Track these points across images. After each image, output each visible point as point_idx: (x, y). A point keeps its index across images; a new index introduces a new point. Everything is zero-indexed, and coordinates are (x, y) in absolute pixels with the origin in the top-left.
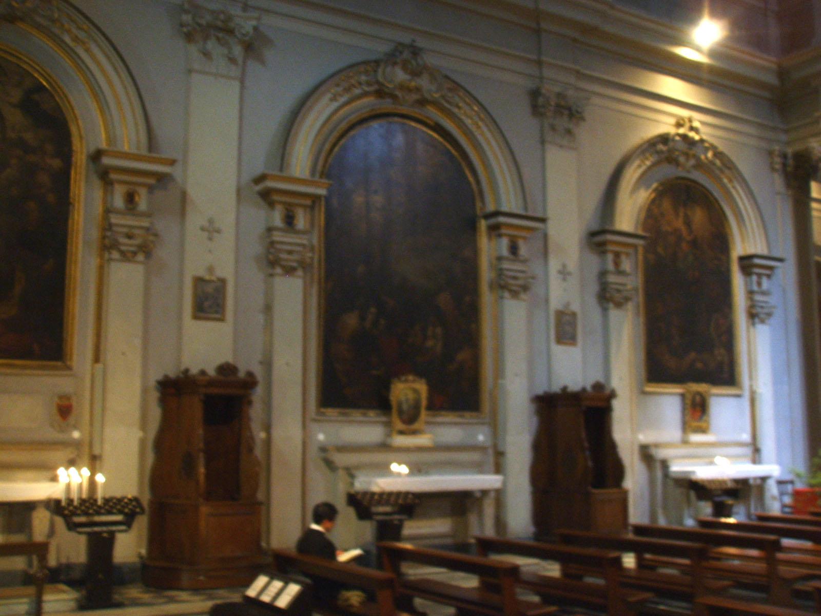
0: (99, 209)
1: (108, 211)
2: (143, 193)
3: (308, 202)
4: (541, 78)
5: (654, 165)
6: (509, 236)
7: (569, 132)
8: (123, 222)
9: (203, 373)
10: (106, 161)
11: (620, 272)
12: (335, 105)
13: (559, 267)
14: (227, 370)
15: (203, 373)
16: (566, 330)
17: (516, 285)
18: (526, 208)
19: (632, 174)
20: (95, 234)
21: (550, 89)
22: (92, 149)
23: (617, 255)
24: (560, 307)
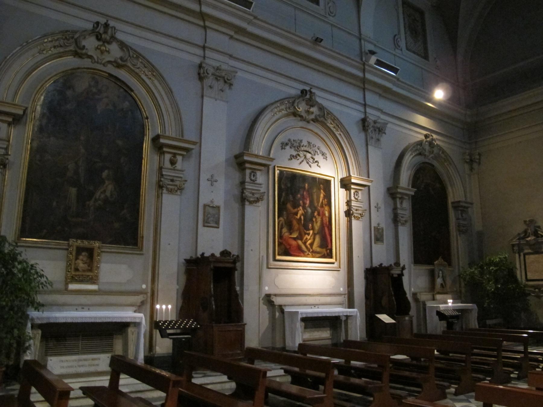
0: (156, 166)
1: (161, 168)
2: (179, 158)
3: (10, 120)
4: (204, 57)
5: (415, 156)
6: (250, 168)
7: (378, 140)
8: (401, 213)
9: (213, 255)
10: (162, 141)
11: (403, 209)
12: (40, 57)
13: (209, 177)
14: (225, 253)
15: (213, 255)
16: (211, 218)
17: (357, 213)
18: (182, 136)
19: (408, 159)
20: (155, 179)
21: (371, 118)
22: (154, 135)
23: (357, 191)
24: (376, 225)
